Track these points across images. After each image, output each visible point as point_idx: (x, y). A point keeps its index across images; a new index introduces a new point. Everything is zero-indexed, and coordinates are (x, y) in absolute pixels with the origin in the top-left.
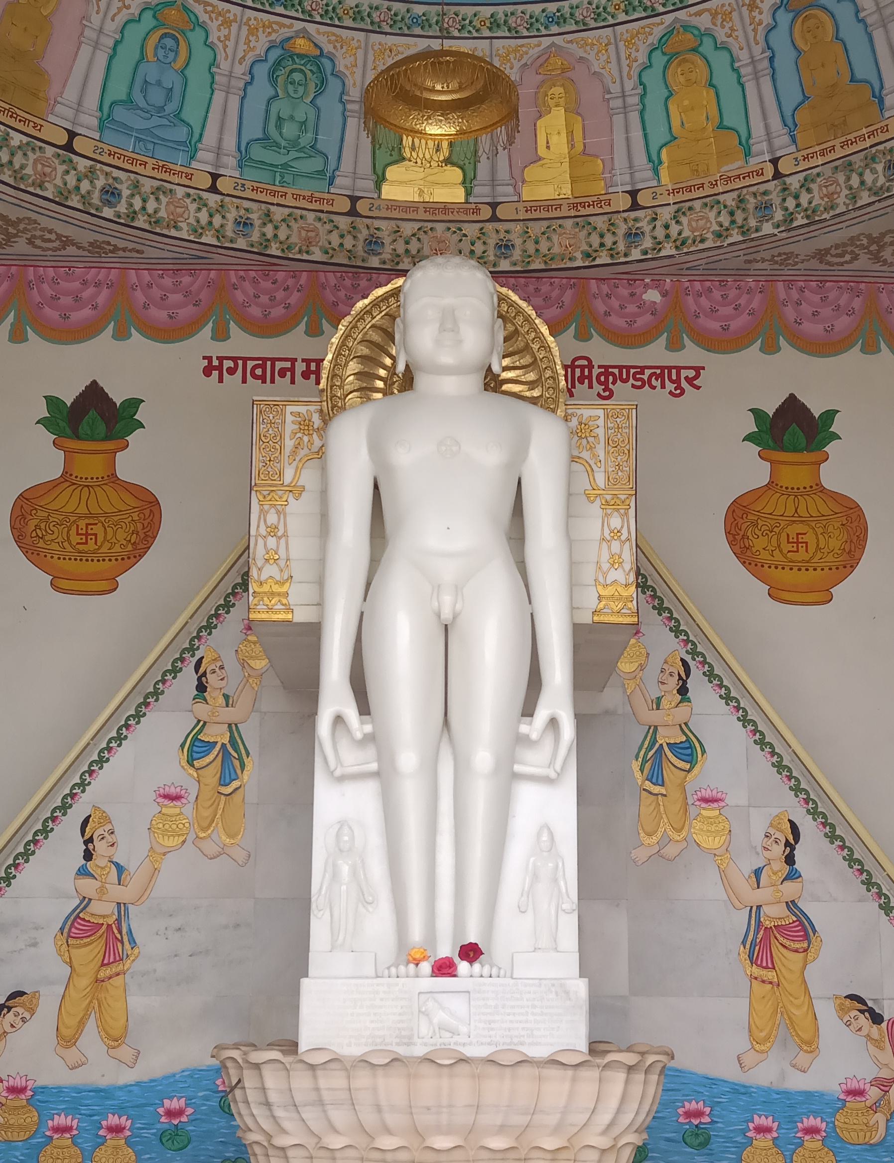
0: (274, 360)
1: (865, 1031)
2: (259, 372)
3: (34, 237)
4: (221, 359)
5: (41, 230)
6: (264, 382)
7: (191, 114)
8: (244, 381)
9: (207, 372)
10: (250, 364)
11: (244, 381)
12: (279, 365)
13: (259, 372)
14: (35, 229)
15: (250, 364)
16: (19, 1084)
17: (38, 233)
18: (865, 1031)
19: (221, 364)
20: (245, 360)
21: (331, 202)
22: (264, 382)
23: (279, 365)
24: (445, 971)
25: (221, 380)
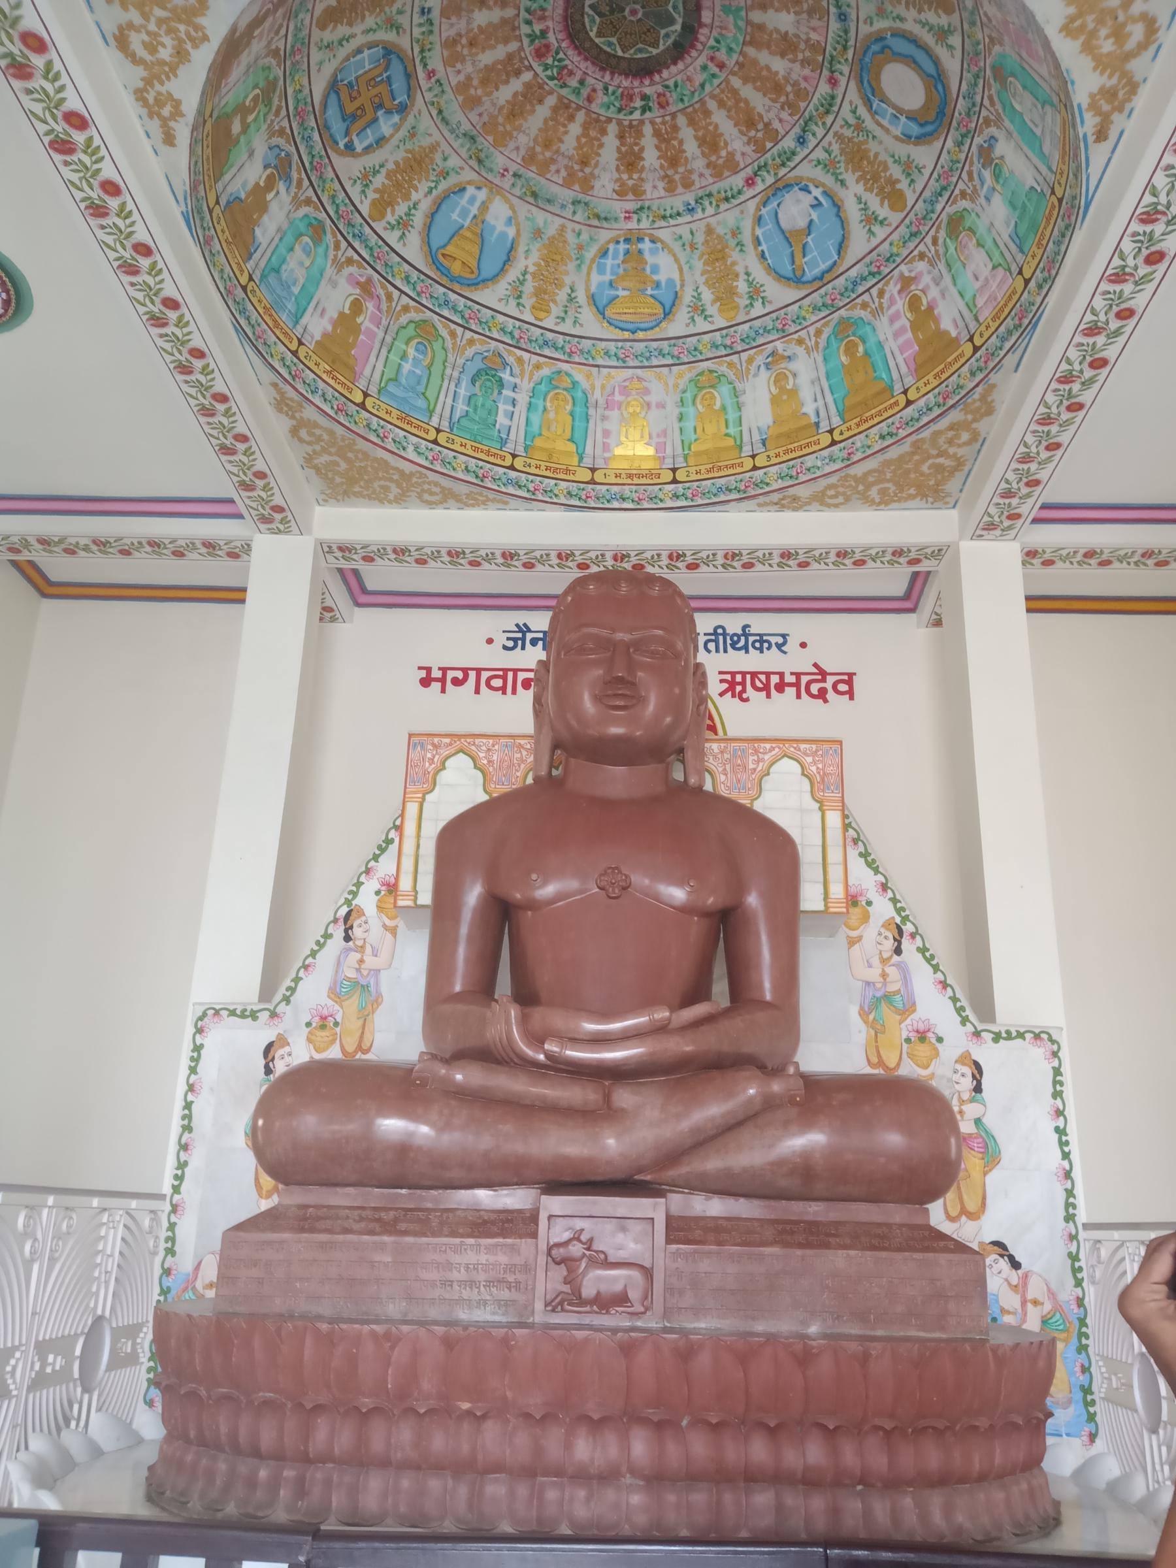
0: (515, 671)
1: (1004, 1275)
2: (497, 683)
3: (423, 491)
4: (444, 670)
5: (429, 483)
6: (504, 693)
7: (431, 394)
8: (477, 691)
9: (426, 682)
10: (485, 675)
11: (477, 691)
12: (522, 676)
13: (757, 645)
14: (424, 483)
15: (485, 675)
16: (968, 1525)
17: (426, 487)
18: (1004, 1275)
19: (444, 675)
20: (479, 671)
21: (741, 465)
22: (504, 693)
23: (522, 676)
24: (502, 1216)
25: (443, 691)
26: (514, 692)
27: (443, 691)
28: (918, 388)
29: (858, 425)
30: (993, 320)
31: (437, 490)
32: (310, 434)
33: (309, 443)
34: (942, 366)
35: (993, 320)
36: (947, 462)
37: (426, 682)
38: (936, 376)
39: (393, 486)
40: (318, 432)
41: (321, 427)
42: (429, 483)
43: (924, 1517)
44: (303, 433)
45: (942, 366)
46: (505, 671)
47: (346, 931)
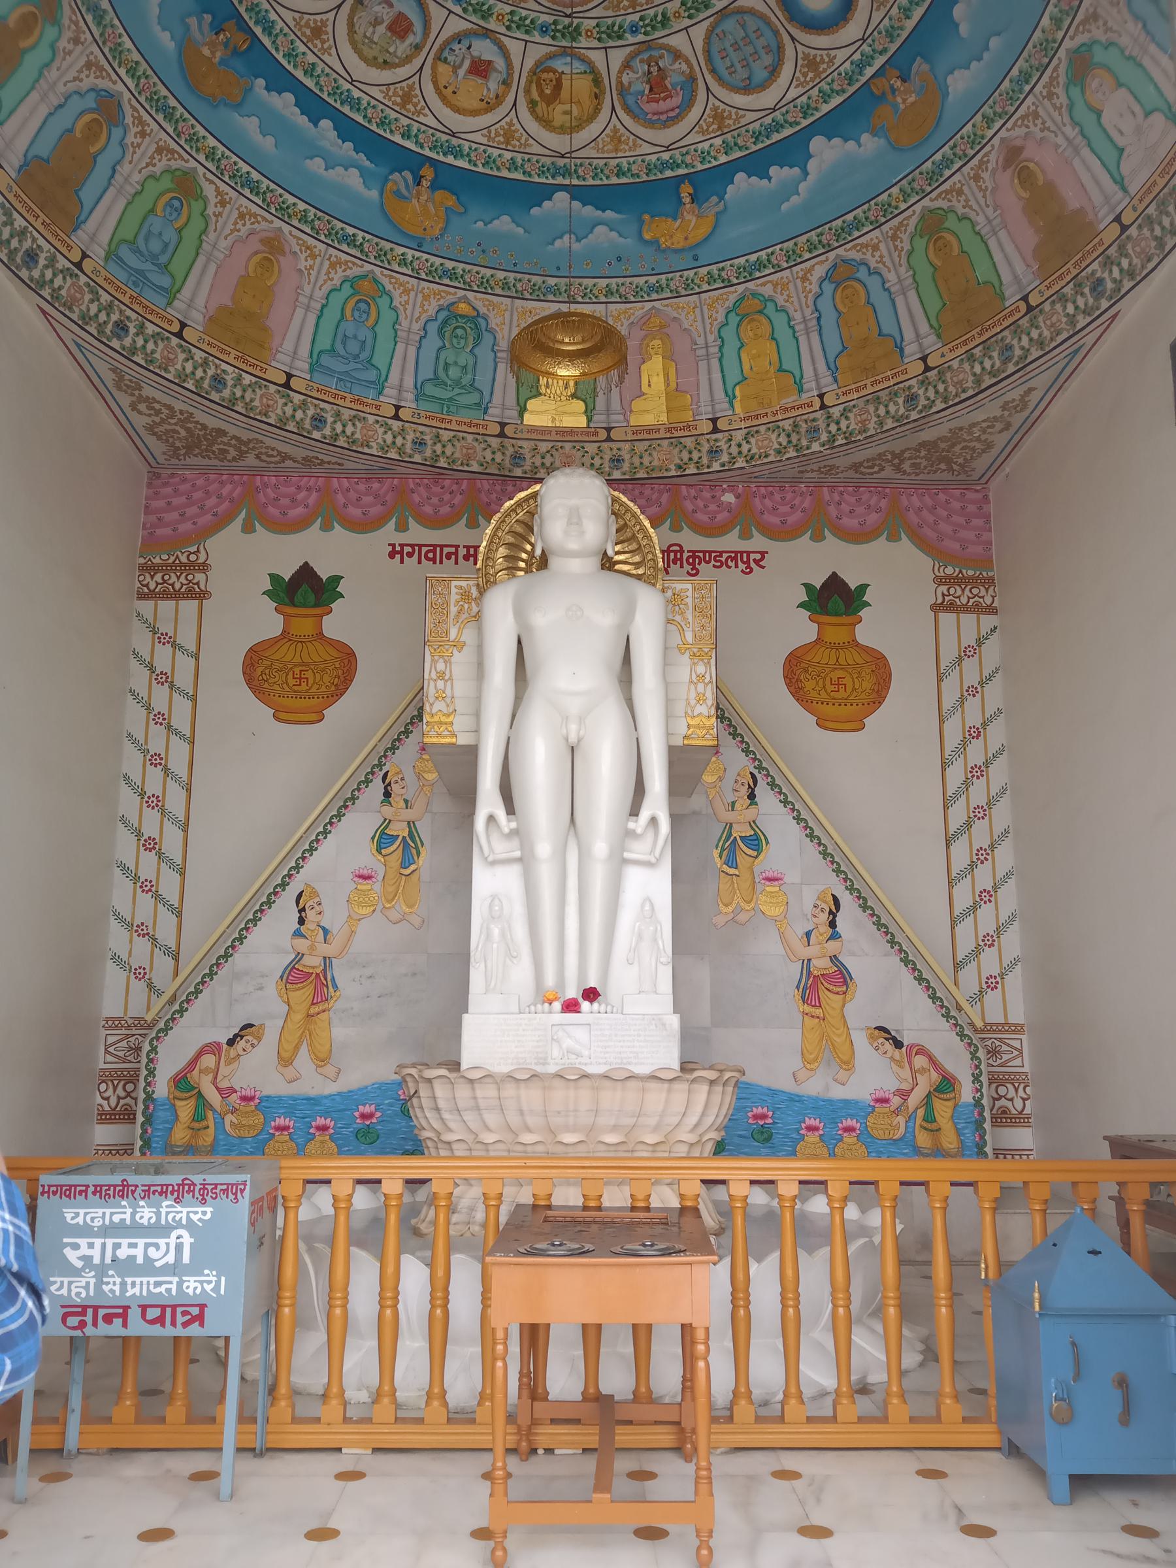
0: (442, 547)
6: (435, 563)
8: (420, 562)
9: (391, 556)
10: (424, 549)
11: (420, 562)
15: (424, 549)
19: (402, 549)
22: (435, 563)
25: (402, 561)
26: (441, 563)
27: (402, 561)
28: (1040, 292)
29: (980, 334)
30: (1161, 175)
31: (275, 453)
32: (150, 408)
33: (150, 415)
34: (1080, 255)
35: (1161, 175)
36: (978, 446)
37: (391, 556)
38: (1076, 264)
39: (231, 450)
40: (157, 406)
41: (158, 402)
42: (267, 448)
43: (349, 357)
44: (142, 407)
45: (1080, 255)
46: (435, 546)
47: (236, 1036)
